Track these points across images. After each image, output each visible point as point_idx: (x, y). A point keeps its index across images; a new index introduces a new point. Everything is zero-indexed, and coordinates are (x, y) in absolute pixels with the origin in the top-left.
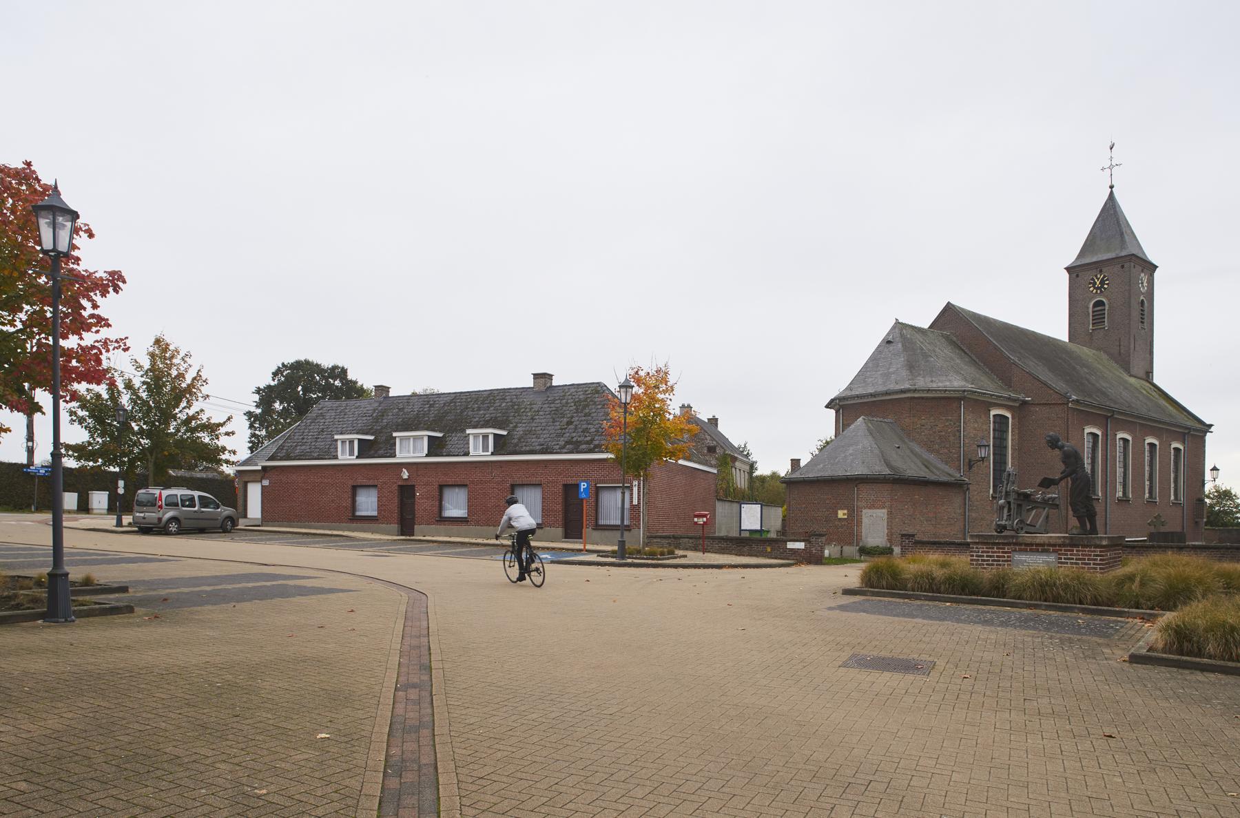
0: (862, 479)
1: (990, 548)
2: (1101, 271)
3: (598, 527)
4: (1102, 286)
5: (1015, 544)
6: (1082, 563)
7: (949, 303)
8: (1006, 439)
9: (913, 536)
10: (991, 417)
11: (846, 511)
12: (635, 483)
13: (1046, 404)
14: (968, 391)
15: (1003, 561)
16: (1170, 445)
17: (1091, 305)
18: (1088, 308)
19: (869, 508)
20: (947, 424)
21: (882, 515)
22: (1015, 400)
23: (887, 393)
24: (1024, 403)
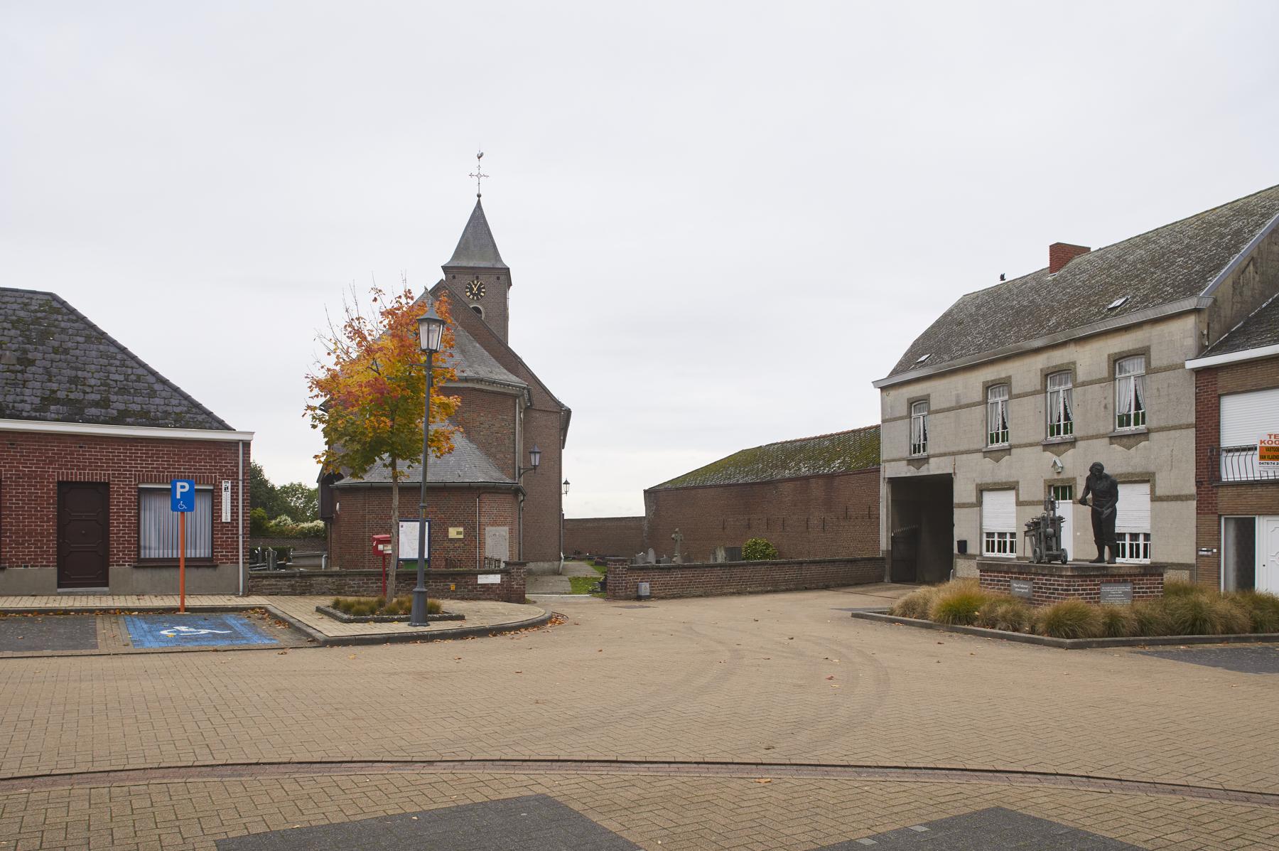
0: (485, 487)
2: (477, 278)
3: (144, 564)
4: (479, 294)
5: (1104, 576)
11: (461, 529)
12: (226, 484)
19: (492, 526)
21: (504, 534)
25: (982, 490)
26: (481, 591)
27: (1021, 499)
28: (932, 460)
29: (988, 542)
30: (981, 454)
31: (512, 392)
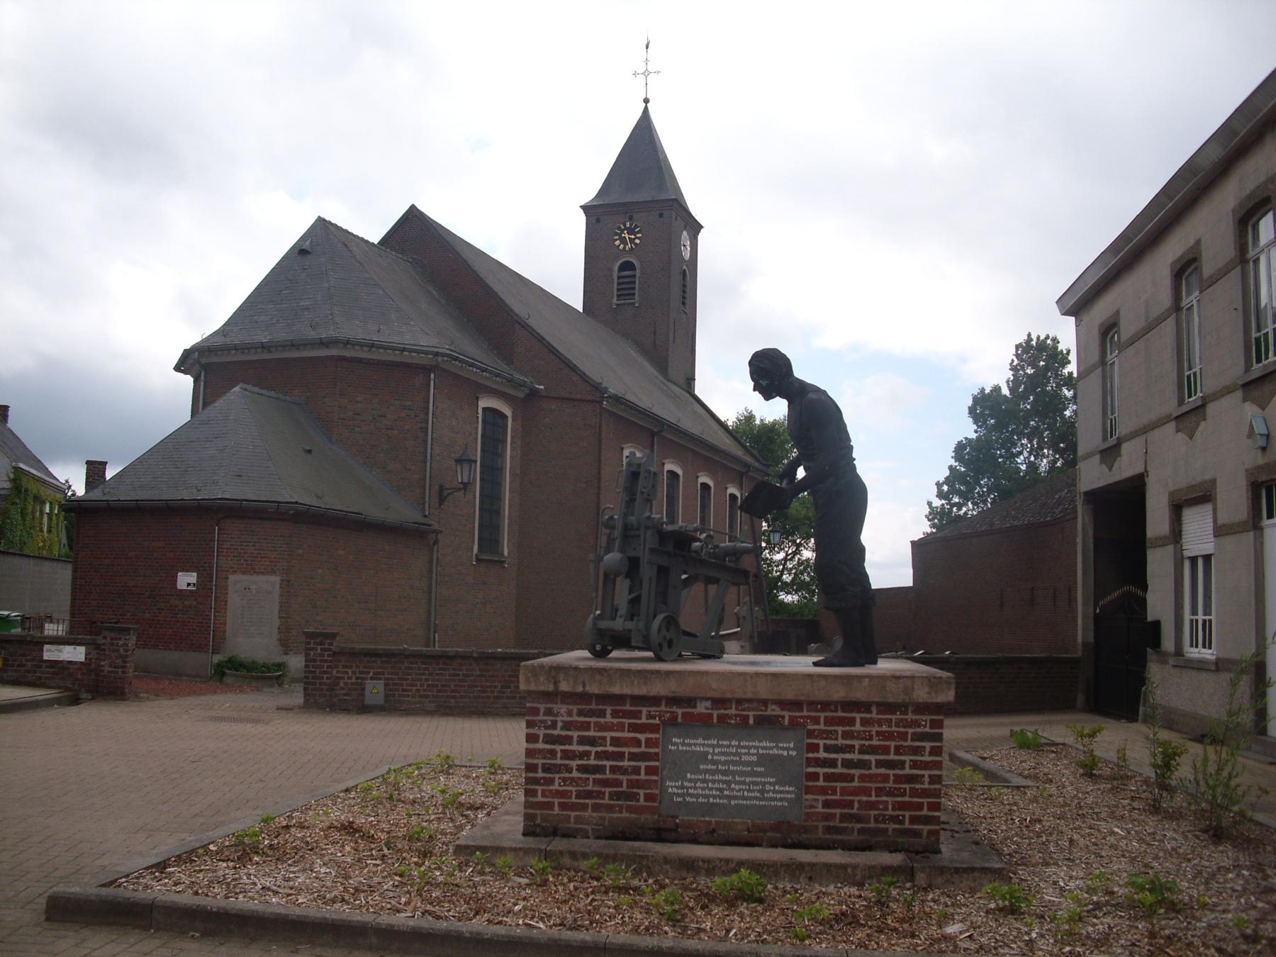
1: (591, 713)
2: (631, 218)
4: (620, 235)
6: (880, 764)
7: (413, 207)
8: (503, 455)
9: (334, 636)
10: (480, 411)
13: (567, 399)
14: (444, 355)
15: (633, 757)
16: (726, 488)
17: (616, 268)
18: (611, 270)
19: (244, 573)
20: (403, 415)
22: (520, 385)
23: (293, 345)
24: (534, 394)
25: (1177, 508)
26: (48, 673)
27: (1220, 522)
28: (1125, 447)
29: (1192, 621)
30: (1171, 426)
31: (402, 360)
